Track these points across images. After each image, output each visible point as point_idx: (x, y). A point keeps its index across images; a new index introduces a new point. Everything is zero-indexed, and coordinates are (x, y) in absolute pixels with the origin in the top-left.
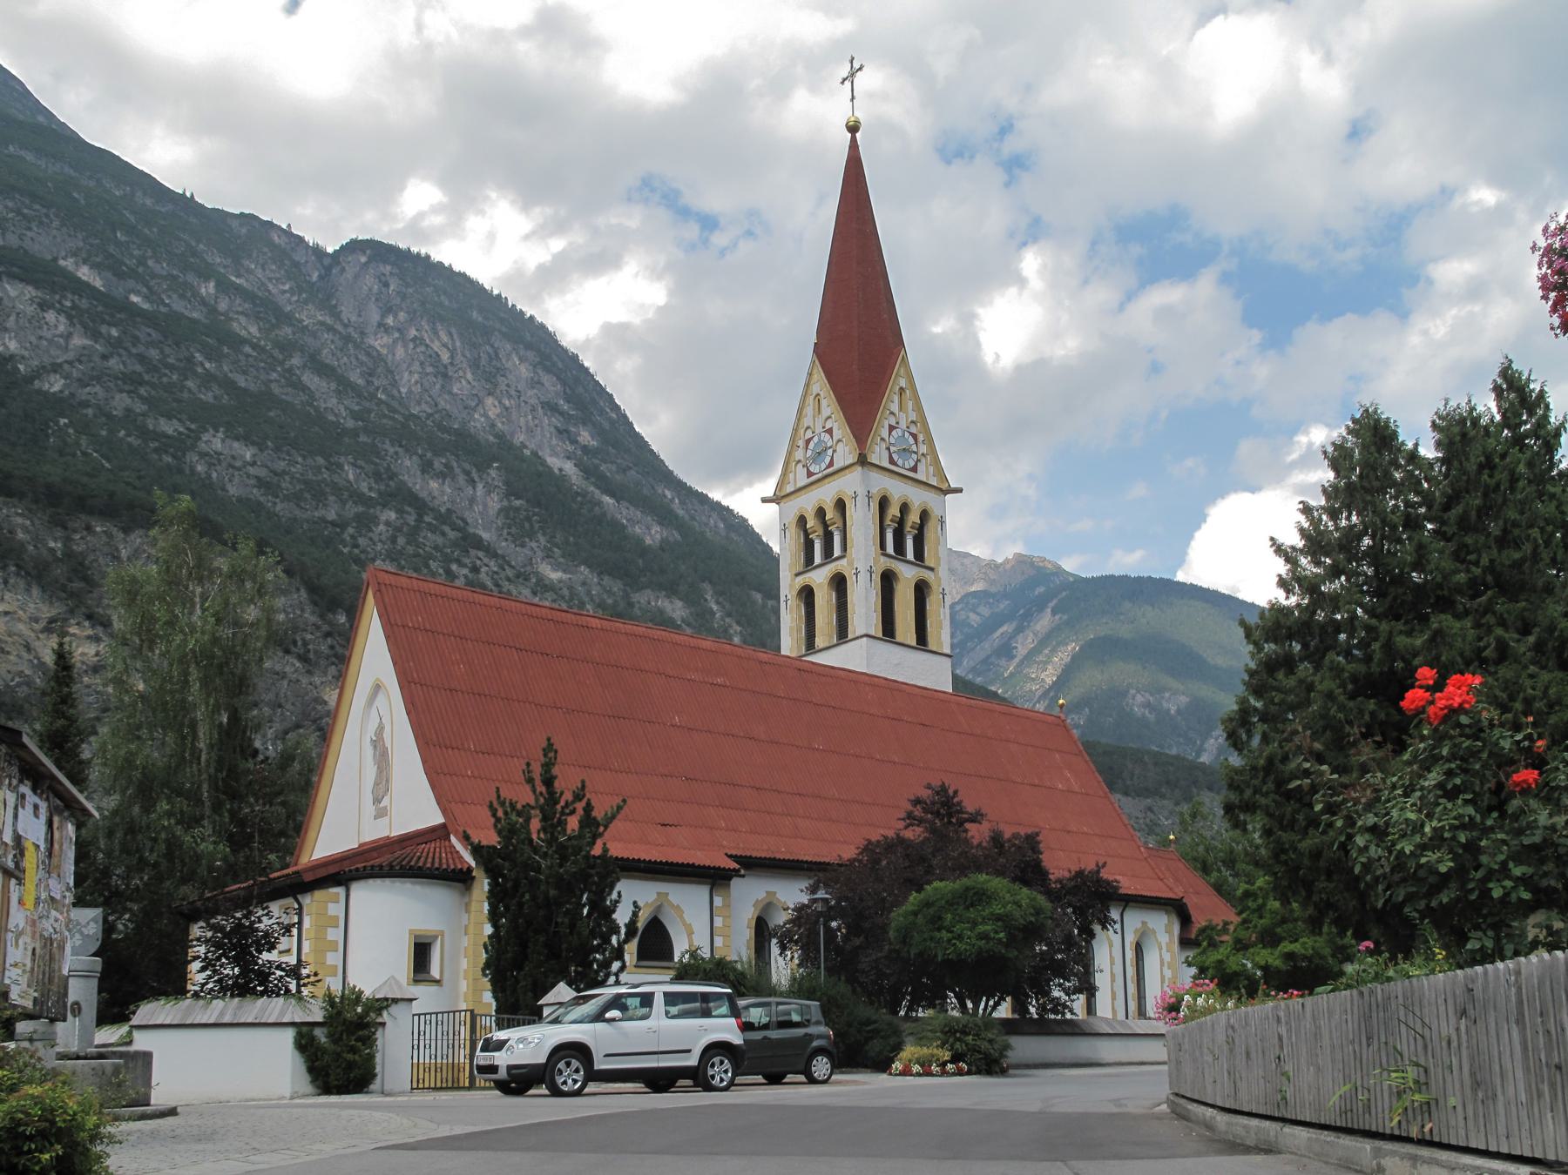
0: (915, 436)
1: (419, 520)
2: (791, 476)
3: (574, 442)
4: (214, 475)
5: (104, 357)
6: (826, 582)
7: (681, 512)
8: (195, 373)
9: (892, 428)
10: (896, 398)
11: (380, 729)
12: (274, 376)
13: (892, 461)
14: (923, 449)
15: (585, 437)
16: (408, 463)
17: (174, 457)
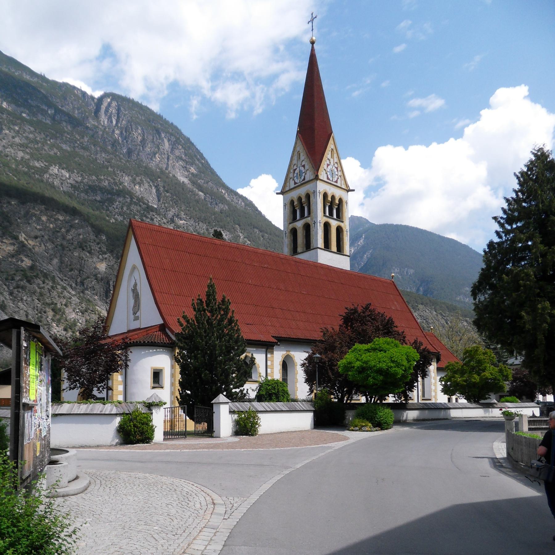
0: (337, 168)
1: (131, 200)
2: (288, 184)
3: (188, 171)
4: (55, 182)
5: (13, 137)
6: (302, 226)
7: (228, 199)
8: (47, 143)
9: (328, 165)
10: (330, 153)
11: (136, 285)
12: (76, 145)
13: (328, 178)
14: (340, 174)
15: (193, 170)
16: (126, 178)
17: (40, 176)
